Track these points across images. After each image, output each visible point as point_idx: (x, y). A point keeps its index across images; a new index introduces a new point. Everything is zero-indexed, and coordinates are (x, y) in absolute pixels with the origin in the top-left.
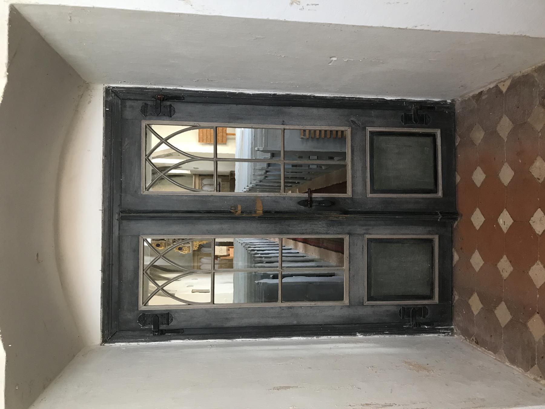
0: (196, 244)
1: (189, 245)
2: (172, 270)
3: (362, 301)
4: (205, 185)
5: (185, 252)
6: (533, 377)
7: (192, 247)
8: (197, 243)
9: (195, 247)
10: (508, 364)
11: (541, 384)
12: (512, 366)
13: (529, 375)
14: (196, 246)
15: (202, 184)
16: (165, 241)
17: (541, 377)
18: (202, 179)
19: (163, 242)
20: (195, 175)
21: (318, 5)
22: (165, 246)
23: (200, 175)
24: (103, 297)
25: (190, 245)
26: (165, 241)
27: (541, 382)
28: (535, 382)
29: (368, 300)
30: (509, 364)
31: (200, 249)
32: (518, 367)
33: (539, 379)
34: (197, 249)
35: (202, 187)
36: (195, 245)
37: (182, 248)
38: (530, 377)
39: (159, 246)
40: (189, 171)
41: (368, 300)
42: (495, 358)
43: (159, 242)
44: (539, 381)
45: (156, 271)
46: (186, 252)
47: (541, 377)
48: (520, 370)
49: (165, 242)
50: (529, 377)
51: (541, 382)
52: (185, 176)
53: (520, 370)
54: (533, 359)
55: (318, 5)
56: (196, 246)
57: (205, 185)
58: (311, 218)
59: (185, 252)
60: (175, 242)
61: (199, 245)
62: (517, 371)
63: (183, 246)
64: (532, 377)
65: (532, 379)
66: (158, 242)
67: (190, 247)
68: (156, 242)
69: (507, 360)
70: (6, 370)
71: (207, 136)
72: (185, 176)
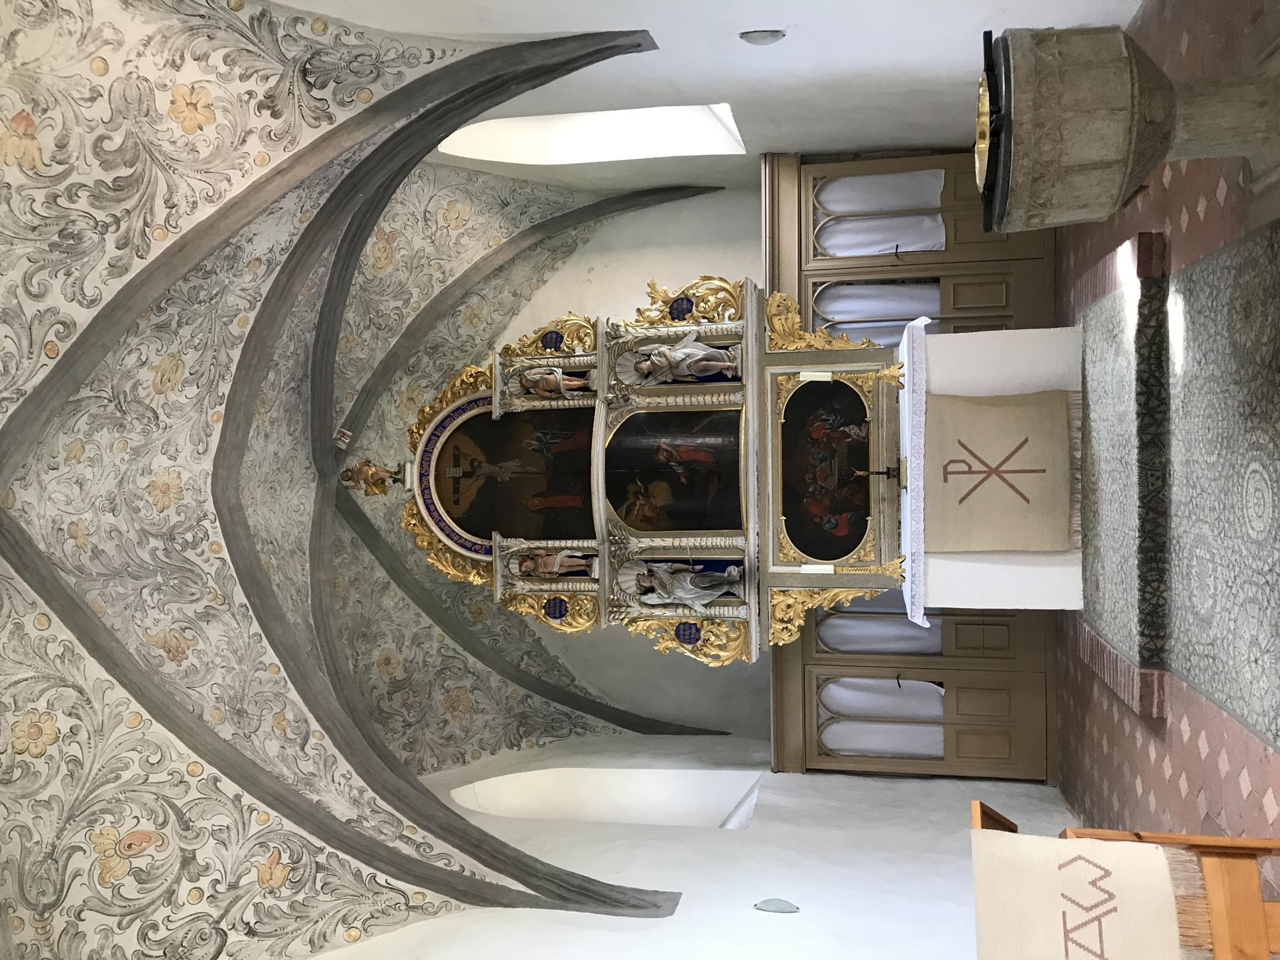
0: (789, 606)
1: (741, 612)
2: (670, 724)
4: (840, 219)
5: (717, 657)
7: (764, 628)
8: (791, 601)
9: (780, 626)
14: (790, 621)
15: (821, 210)
16: (596, 581)
18: (820, 185)
19: (578, 586)
20: (773, 158)
22: (595, 614)
23: (805, 159)
25: (747, 612)
26: (596, 581)
29: (772, 374)
31: (818, 624)
34: (796, 636)
35: (817, 237)
36: (779, 615)
37: (698, 631)
39: (561, 616)
40: (724, 110)
41: (772, 374)
43: (560, 586)
45: (585, 727)
46: (722, 654)
49: (596, 587)
52: (723, 188)
56: (790, 621)
57: (840, 219)
59: (717, 657)
60: (651, 590)
61: (809, 611)
63: (707, 618)
66: (554, 586)
67: (746, 623)
68: (546, 587)
71: (914, 384)
72: (723, 188)
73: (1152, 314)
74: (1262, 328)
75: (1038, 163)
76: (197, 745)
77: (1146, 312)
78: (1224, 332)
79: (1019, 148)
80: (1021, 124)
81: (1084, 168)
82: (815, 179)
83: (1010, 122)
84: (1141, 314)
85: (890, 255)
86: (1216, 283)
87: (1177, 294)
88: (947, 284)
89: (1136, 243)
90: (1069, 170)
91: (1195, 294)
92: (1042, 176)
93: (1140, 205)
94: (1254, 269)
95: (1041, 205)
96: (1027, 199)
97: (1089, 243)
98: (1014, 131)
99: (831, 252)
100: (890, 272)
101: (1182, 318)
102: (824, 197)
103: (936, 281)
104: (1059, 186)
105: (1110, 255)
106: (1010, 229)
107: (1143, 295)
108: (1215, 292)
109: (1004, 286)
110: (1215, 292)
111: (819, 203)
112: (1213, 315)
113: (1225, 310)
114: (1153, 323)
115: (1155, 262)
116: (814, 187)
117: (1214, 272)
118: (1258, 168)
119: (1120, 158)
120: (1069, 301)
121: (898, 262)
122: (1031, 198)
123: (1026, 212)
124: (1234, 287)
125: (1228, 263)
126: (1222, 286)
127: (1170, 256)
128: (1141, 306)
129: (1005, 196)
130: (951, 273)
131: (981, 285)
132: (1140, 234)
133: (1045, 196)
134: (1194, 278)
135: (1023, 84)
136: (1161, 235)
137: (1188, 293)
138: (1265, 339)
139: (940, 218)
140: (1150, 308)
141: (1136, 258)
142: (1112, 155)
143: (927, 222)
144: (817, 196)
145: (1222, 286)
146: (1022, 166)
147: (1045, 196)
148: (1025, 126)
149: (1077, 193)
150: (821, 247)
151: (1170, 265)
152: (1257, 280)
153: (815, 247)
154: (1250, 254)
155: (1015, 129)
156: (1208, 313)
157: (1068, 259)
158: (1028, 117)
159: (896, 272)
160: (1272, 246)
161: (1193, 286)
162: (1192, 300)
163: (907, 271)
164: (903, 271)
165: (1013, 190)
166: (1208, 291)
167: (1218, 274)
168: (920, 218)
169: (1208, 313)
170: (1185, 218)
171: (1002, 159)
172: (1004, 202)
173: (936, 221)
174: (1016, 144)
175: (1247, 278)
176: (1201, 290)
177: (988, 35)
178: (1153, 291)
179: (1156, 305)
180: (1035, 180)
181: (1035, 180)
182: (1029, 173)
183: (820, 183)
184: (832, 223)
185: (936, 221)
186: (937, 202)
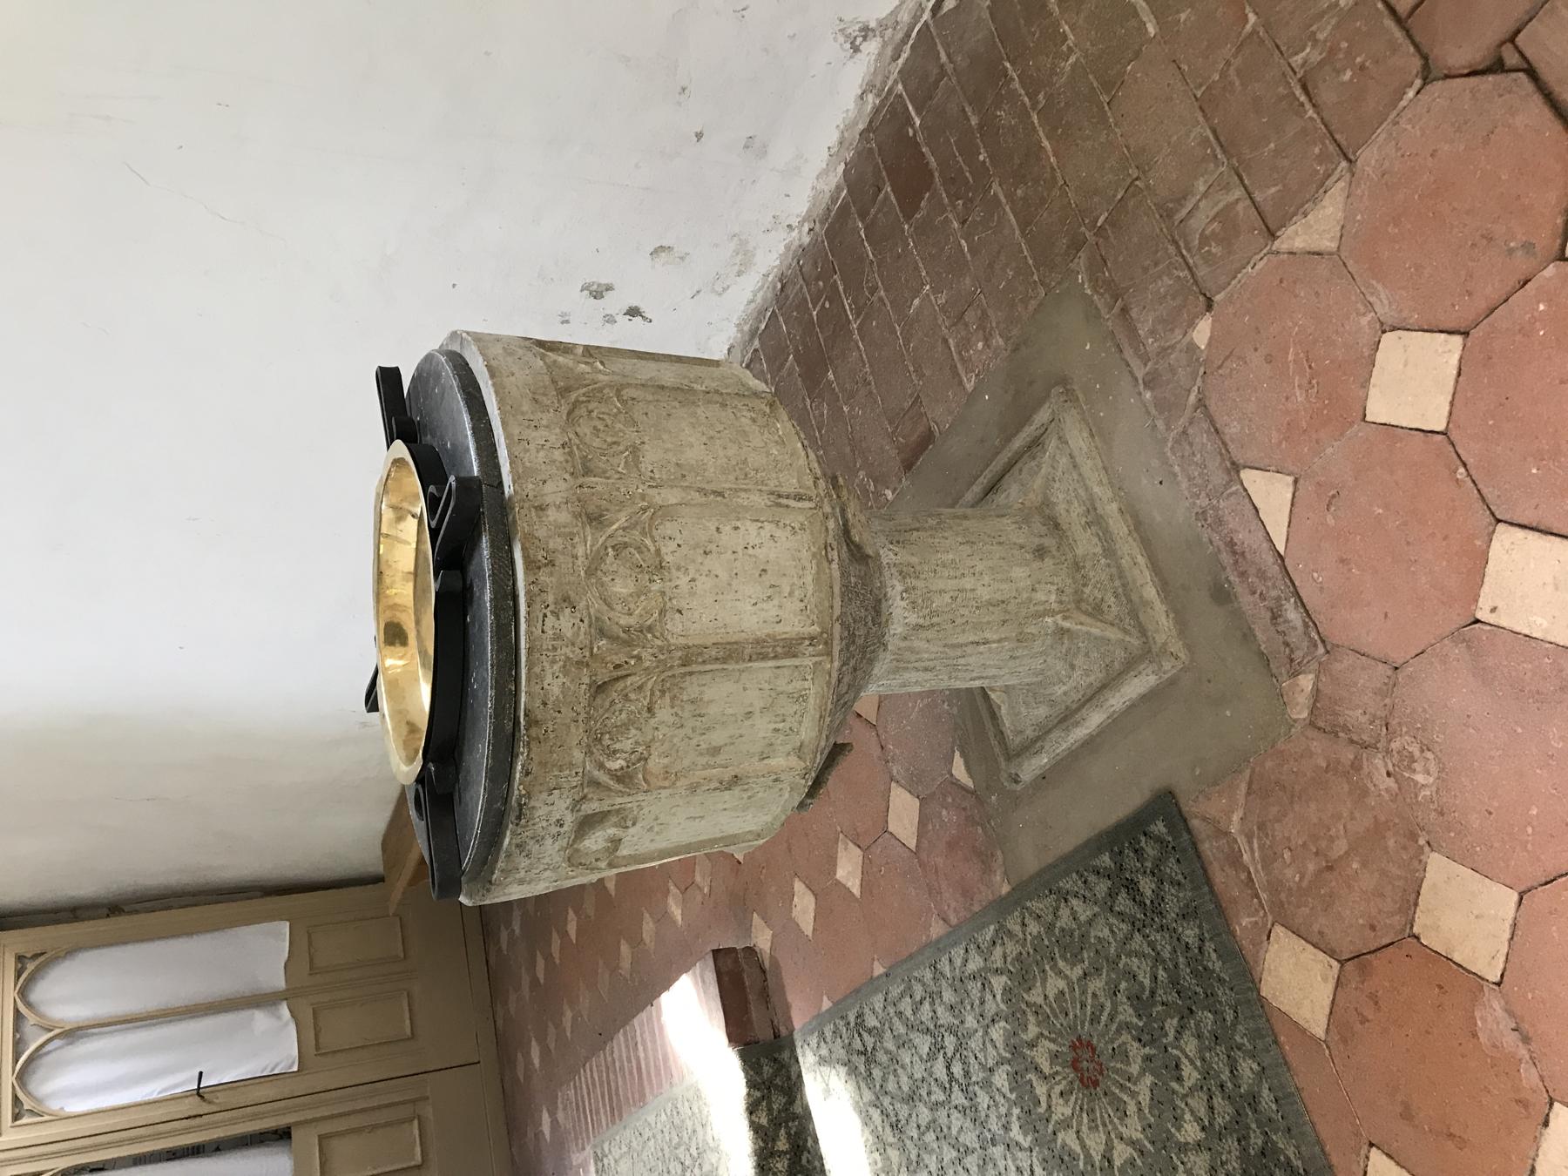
4: (73, 1034)
15: (31, 1019)
35: (22, 1077)
57: (73, 1034)
73: (776, 1123)
74: (1162, 1101)
75: (602, 633)
76: (927, 664)
77: (764, 1121)
78: (1016, 1133)
79: (543, 577)
80: (541, 508)
81: (732, 653)
82: (20, 958)
83: (503, 507)
84: (755, 1128)
85: (186, 1095)
86: (945, 1017)
87: (825, 1070)
88: (305, 1139)
89: (711, 977)
90: (691, 657)
91: (882, 1057)
92: (620, 674)
93: (676, 912)
94: (1075, 959)
95: (623, 777)
96: (578, 755)
97: (569, 1014)
98: (522, 526)
99: (54, 1105)
100: (187, 1131)
101: (855, 1121)
102: (39, 993)
103: (282, 1136)
104: (664, 714)
105: (643, 1015)
106: (514, 887)
107: (751, 1084)
108: (950, 1042)
109: (416, 1122)
110: (950, 1042)
111: (29, 1005)
112: (958, 1098)
113: (1001, 1079)
114: (782, 1145)
115: (755, 1013)
116: (18, 974)
117: (933, 996)
118: (1018, 718)
119: (816, 629)
120: (538, 1135)
121: (206, 1108)
122: (589, 752)
123: (575, 806)
124: (1016, 1018)
125: (975, 964)
126: (971, 1022)
127: (781, 989)
128: (752, 1109)
129: (506, 746)
130: (309, 1115)
131: (374, 1128)
132: (716, 953)
133: (627, 745)
134: (871, 1022)
135: (526, 406)
136: (751, 951)
137: (860, 1062)
138: (1191, 1132)
139: (284, 1011)
140: (770, 1109)
141: (717, 1005)
142: (794, 624)
143: (260, 1019)
144: (23, 993)
145: (971, 1022)
146: (558, 637)
147: (627, 745)
148: (552, 514)
149: (718, 737)
150: (29, 1094)
151: (787, 1007)
152: (1096, 985)
153: (16, 1099)
154: (1050, 928)
155: (523, 521)
156: (939, 1096)
157: (527, 1055)
158: (556, 490)
159: (200, 1128)
160: (1132, 887)
161: (869, 1041)
162: (877, 1073)
163: (223, 1124)
164: (215, 1125)
165: (532, 722)
166: (924, 1044)
167: (948, 996)
168: (244, 1015)
169: (939, 1096)
170: (804, 906)
171: (489, 619)
172: (501, 773)
173: (279, 1018)
174: (530, 564)
175: (1055, 984)
176: (903, 1044)
177: (388, 379)
178: (767, 1070)
179: (778, 1101)
180: (599, 689)
181: (599, 689)
182: (580, 664)
183: (31, 967)
184: (57, 1043)
185: (279, 1018)
186: (280, 983)
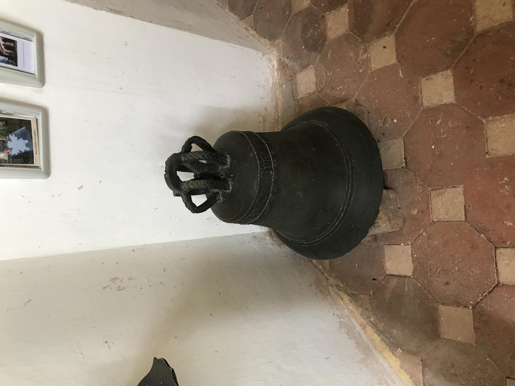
3: (426, 369)
6: (245, 26)
10: (227, 10)
11: (250, 33)
12: (230, 13)
13: (242, 24)
17: (252, 27)
21: (30, 300)
24: (26, 151)
27: (250, 32)
28: (245, 30)
30: (228, 11)
32: (235, 14)
33: (249, 28)
38: (242, 25)
42: (217, 3)
44: (249, 30)
47: (252, 27)
48: (236, 18)
50: (241, 26)
51: (250, 32)
53: (236, 17)
54: (252, 9)
55: (30, 300)
58: (351, 194)
62: (233, 17)
64: (244, 26)
65: (243, 28)
69: (228, 7)
70: (142, 380)
